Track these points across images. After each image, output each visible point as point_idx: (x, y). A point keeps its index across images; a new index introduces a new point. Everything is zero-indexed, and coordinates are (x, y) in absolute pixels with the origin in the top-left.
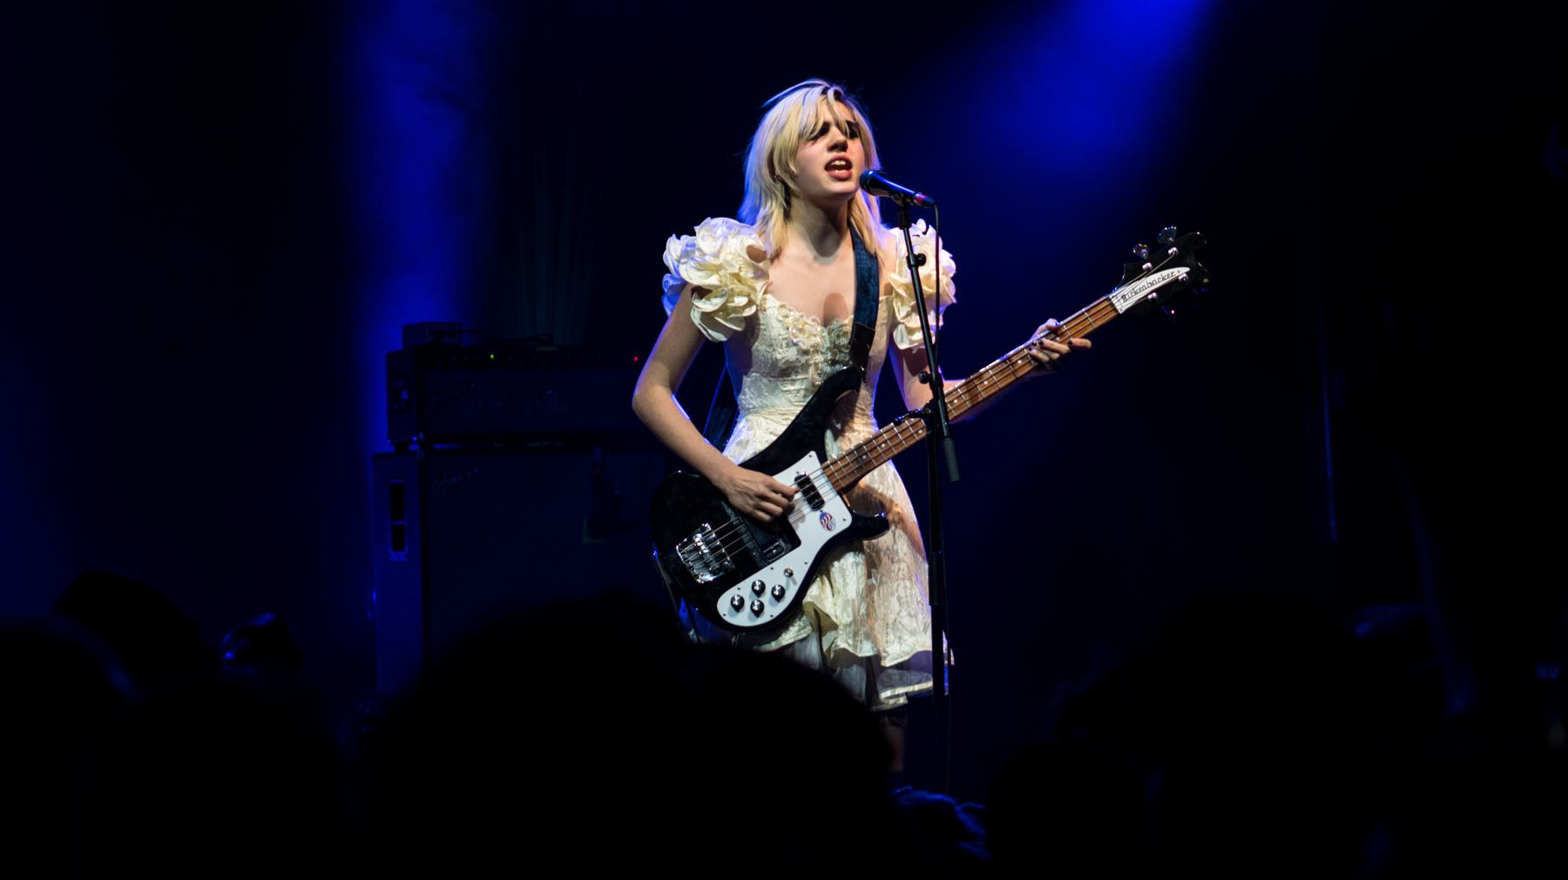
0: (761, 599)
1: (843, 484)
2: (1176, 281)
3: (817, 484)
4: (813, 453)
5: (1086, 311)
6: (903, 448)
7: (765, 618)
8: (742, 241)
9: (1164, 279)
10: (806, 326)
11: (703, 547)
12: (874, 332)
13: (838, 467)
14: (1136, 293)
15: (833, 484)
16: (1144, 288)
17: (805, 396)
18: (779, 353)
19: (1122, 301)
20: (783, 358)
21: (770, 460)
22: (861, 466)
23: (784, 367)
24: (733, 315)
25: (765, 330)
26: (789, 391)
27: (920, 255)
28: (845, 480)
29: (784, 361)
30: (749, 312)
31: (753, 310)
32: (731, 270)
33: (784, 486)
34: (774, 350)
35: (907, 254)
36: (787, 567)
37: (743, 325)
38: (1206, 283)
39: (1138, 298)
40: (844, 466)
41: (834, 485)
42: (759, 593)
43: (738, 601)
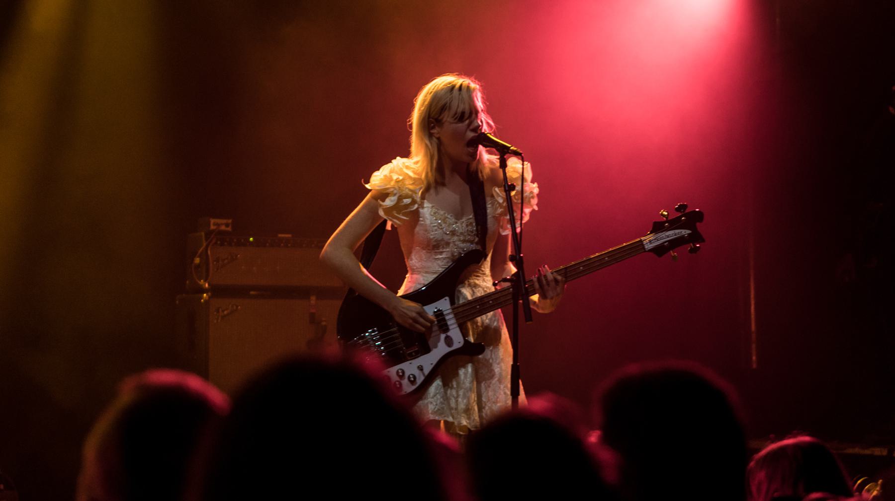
6: (214, 220)
17: (448, 262)
18: (432, 235)
20: (434, 237)
21: (420, 297)
23: (435, 243)
25: (422, 221)
26: (438, 259)
29: (435, 239)
31: (416, 206)
34: (428, 233)
36: (419, 365)
43: (413, 377)
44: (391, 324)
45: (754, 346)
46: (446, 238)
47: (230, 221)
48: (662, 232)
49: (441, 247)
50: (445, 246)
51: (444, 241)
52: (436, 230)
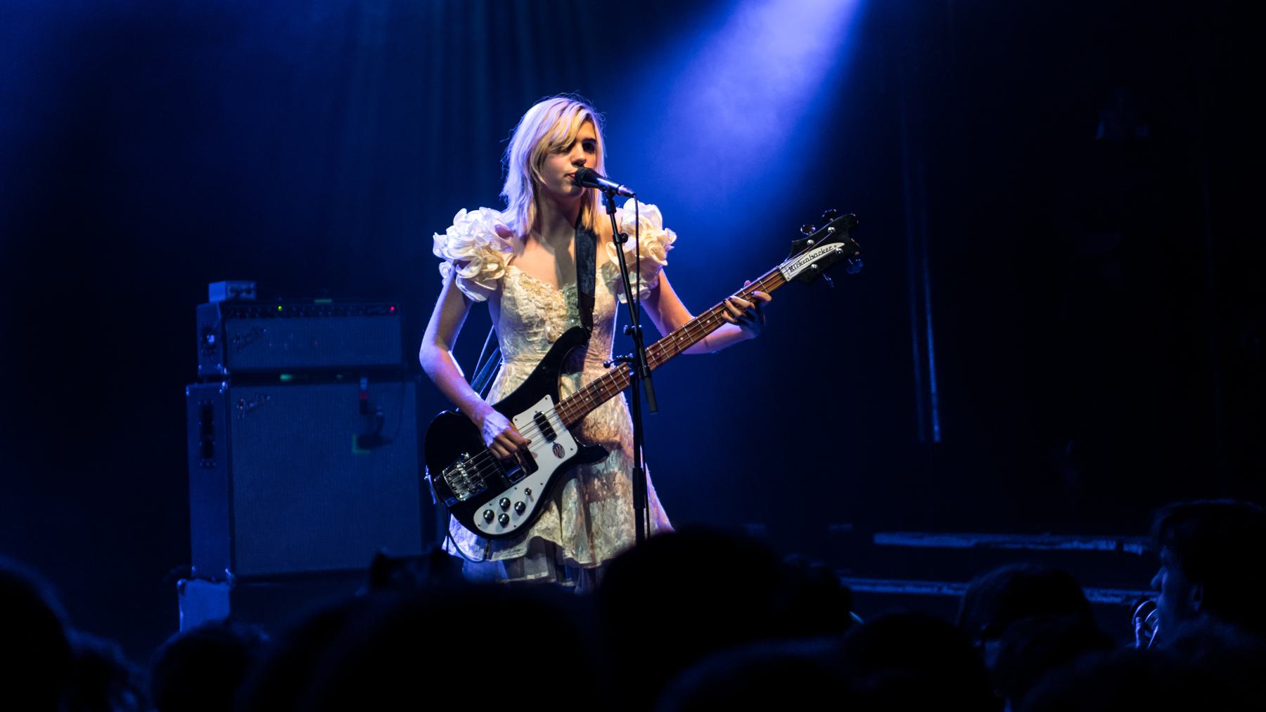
0: (506, 513)
1: (570, 421)
2: (834, 254)
3: (551, 421)
4: (548, 396)
5: (761, 280)
7: (510, 528)
8: (491, 222)
9: (823, 252)
10: (542, 290)
11: (462, 472)
12: (594, 299)
13: (572, 404)
14: (801, 264)
15: (563, 421)
16: (807, 260)
18: (521, 310)
19: (789, 271)
21: (510, 407)
22: (599, 397)
24: (487, 279)
27: (623, 234)
28: (572, 417)
30: (498, 276)
32: (482, 244)
33: (561, 396)
35: (613, 234)
36: (530, 488)
37: (496, 286)
38: (858, 255)
39: (802, 268)
40: (572, 407)
41: (564, 421)
42: (506, 507)
44: (457, 410)
45: (935, 413)
46: (541, 312)
47: (252, 285)
48: (803, 253)
49: (535, 326)
50: (540, 325)
51: (538, 317)
52: (527, 304)
